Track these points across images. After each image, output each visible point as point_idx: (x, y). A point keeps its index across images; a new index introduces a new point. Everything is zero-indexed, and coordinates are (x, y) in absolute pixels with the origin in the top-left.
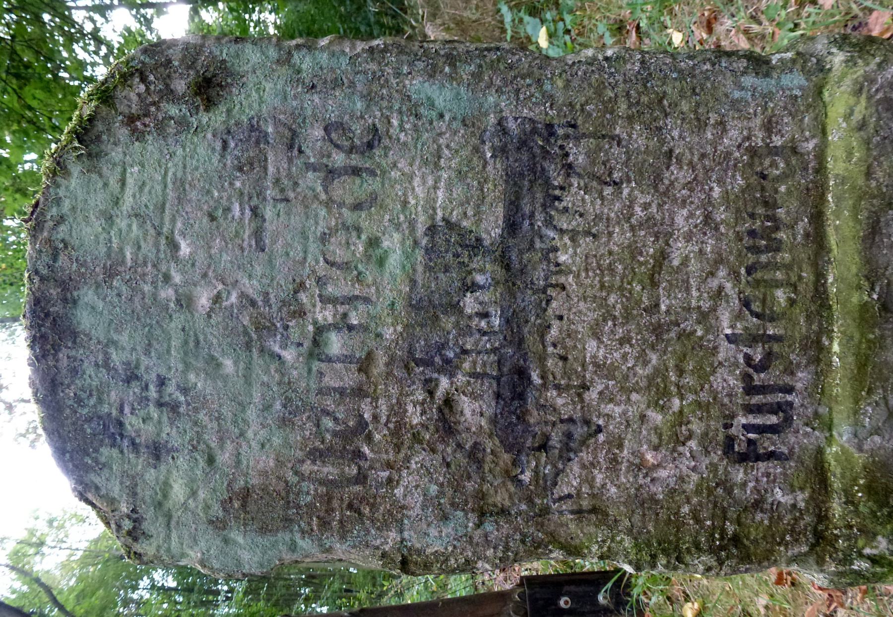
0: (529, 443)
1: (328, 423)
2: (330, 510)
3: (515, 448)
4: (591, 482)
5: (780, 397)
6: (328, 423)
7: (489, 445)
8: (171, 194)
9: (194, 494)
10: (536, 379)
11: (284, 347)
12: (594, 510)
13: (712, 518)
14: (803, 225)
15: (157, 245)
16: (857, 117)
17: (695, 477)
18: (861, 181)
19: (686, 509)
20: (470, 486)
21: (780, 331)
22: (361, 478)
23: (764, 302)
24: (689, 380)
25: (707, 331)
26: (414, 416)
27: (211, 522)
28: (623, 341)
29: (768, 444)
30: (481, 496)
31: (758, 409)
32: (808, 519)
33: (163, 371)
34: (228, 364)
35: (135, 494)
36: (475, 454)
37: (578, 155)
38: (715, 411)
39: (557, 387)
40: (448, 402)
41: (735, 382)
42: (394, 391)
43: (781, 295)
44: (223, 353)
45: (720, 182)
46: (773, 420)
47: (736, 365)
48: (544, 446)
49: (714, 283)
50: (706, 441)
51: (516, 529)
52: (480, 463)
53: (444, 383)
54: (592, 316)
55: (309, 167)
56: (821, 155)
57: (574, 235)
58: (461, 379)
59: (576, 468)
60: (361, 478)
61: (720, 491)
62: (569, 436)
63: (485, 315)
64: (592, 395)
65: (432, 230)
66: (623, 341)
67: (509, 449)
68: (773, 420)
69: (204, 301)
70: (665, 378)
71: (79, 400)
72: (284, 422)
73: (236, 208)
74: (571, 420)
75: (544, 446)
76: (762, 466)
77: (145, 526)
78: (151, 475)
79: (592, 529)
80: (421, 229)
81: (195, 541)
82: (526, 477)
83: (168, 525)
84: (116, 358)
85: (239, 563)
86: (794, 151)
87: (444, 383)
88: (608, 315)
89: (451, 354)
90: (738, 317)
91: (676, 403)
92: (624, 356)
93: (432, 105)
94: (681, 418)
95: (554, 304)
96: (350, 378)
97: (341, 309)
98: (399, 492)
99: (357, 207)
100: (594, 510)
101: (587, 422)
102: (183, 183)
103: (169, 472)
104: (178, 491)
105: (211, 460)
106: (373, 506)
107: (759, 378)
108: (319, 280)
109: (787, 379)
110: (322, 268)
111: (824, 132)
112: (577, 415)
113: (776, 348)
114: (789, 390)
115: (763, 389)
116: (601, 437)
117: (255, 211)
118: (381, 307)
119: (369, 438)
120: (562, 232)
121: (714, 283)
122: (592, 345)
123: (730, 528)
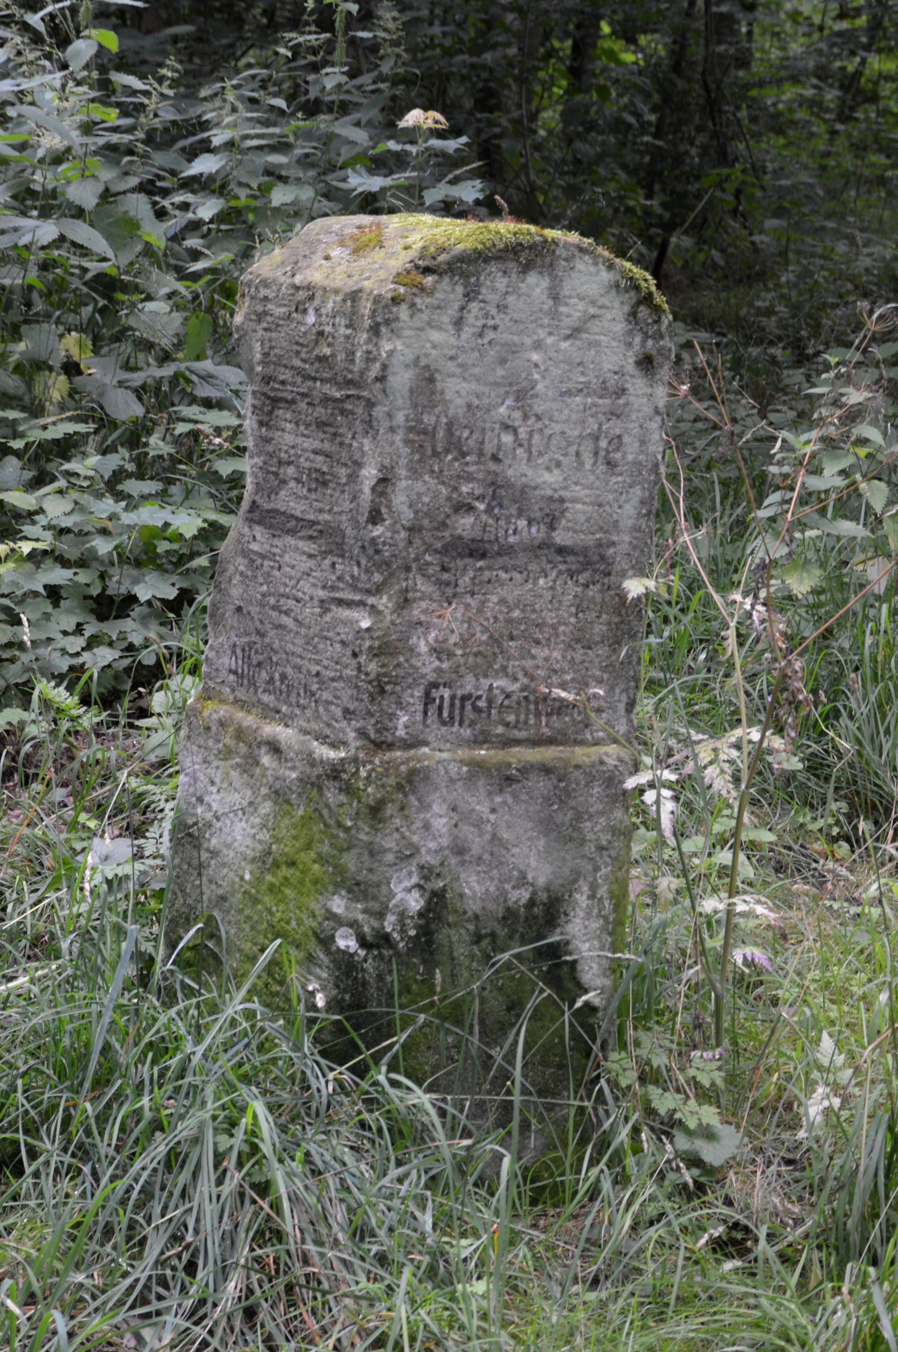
0: (446, 560)
1: (466, 434)
2: (419, 433)
3: (444, 551)
4: (422, 599)
5: (457, 718)
6: (466, 434)
7: (447, 534)
9: (434, 347)
10: (480, 564)
14: (546, 731)
16: (606, 759)
17: (419, 664)
18: (574, 763)
22: (435, 454)
23: (508, 707)
24: (471, 659)
25: (496, 672)
28: (496, 618)
29: (432, 710)
31: (452, 705)
36: (444, 525)
38: (454, 676)
39: (475, 577)
40: (471, 508)
41: (469, 688)
43: (511, 718)
45: (573, 680)
46: (445, 714)
47: (477, 689)
48: (444, 569)
49: (520, 675)
52: (437, 529)
53: (482, 507)
54: (510, 598)
55: (601, 425)
56: (583, 743)
58: (484, 517)
59: (430, 589)
62: (448, 584)
63: (515, 532)
65: (562, 500)
66: (496, 618)
68: (445, 714)
69: (535, 357)
72: (469, 406)
74: (456, 585)
76: (421, 708)
78: (446, 319)
80: (562, 493)
82: (428, 558)
84: (511, 299)
85: (394, 374)
86: (587, 726)
87: (482, 507)
88: (510, 610)
89: (496, 511)
90: (503, 691)
91: (459, 652)
92: (487, 619)
93: (626, 501)
94: (450, 655)
95: (518, 576)
96: (489, 448)
98: (427, 478)
100: (406, 600)
101: (454, 596)
104: (436, 336)
105: (452, 358)
107: (469, 707)
109: (467, 723)
110: (548, 432)
111: (595, 744)
112: (459, 590)
113: (484, 715)
114: (461, 724)
115: (463, 707)
117: (581, 390)
119: (456, 459)
120: (555, 581)
121: (520, 675)
122: (495, 599)
123: (388, 688)
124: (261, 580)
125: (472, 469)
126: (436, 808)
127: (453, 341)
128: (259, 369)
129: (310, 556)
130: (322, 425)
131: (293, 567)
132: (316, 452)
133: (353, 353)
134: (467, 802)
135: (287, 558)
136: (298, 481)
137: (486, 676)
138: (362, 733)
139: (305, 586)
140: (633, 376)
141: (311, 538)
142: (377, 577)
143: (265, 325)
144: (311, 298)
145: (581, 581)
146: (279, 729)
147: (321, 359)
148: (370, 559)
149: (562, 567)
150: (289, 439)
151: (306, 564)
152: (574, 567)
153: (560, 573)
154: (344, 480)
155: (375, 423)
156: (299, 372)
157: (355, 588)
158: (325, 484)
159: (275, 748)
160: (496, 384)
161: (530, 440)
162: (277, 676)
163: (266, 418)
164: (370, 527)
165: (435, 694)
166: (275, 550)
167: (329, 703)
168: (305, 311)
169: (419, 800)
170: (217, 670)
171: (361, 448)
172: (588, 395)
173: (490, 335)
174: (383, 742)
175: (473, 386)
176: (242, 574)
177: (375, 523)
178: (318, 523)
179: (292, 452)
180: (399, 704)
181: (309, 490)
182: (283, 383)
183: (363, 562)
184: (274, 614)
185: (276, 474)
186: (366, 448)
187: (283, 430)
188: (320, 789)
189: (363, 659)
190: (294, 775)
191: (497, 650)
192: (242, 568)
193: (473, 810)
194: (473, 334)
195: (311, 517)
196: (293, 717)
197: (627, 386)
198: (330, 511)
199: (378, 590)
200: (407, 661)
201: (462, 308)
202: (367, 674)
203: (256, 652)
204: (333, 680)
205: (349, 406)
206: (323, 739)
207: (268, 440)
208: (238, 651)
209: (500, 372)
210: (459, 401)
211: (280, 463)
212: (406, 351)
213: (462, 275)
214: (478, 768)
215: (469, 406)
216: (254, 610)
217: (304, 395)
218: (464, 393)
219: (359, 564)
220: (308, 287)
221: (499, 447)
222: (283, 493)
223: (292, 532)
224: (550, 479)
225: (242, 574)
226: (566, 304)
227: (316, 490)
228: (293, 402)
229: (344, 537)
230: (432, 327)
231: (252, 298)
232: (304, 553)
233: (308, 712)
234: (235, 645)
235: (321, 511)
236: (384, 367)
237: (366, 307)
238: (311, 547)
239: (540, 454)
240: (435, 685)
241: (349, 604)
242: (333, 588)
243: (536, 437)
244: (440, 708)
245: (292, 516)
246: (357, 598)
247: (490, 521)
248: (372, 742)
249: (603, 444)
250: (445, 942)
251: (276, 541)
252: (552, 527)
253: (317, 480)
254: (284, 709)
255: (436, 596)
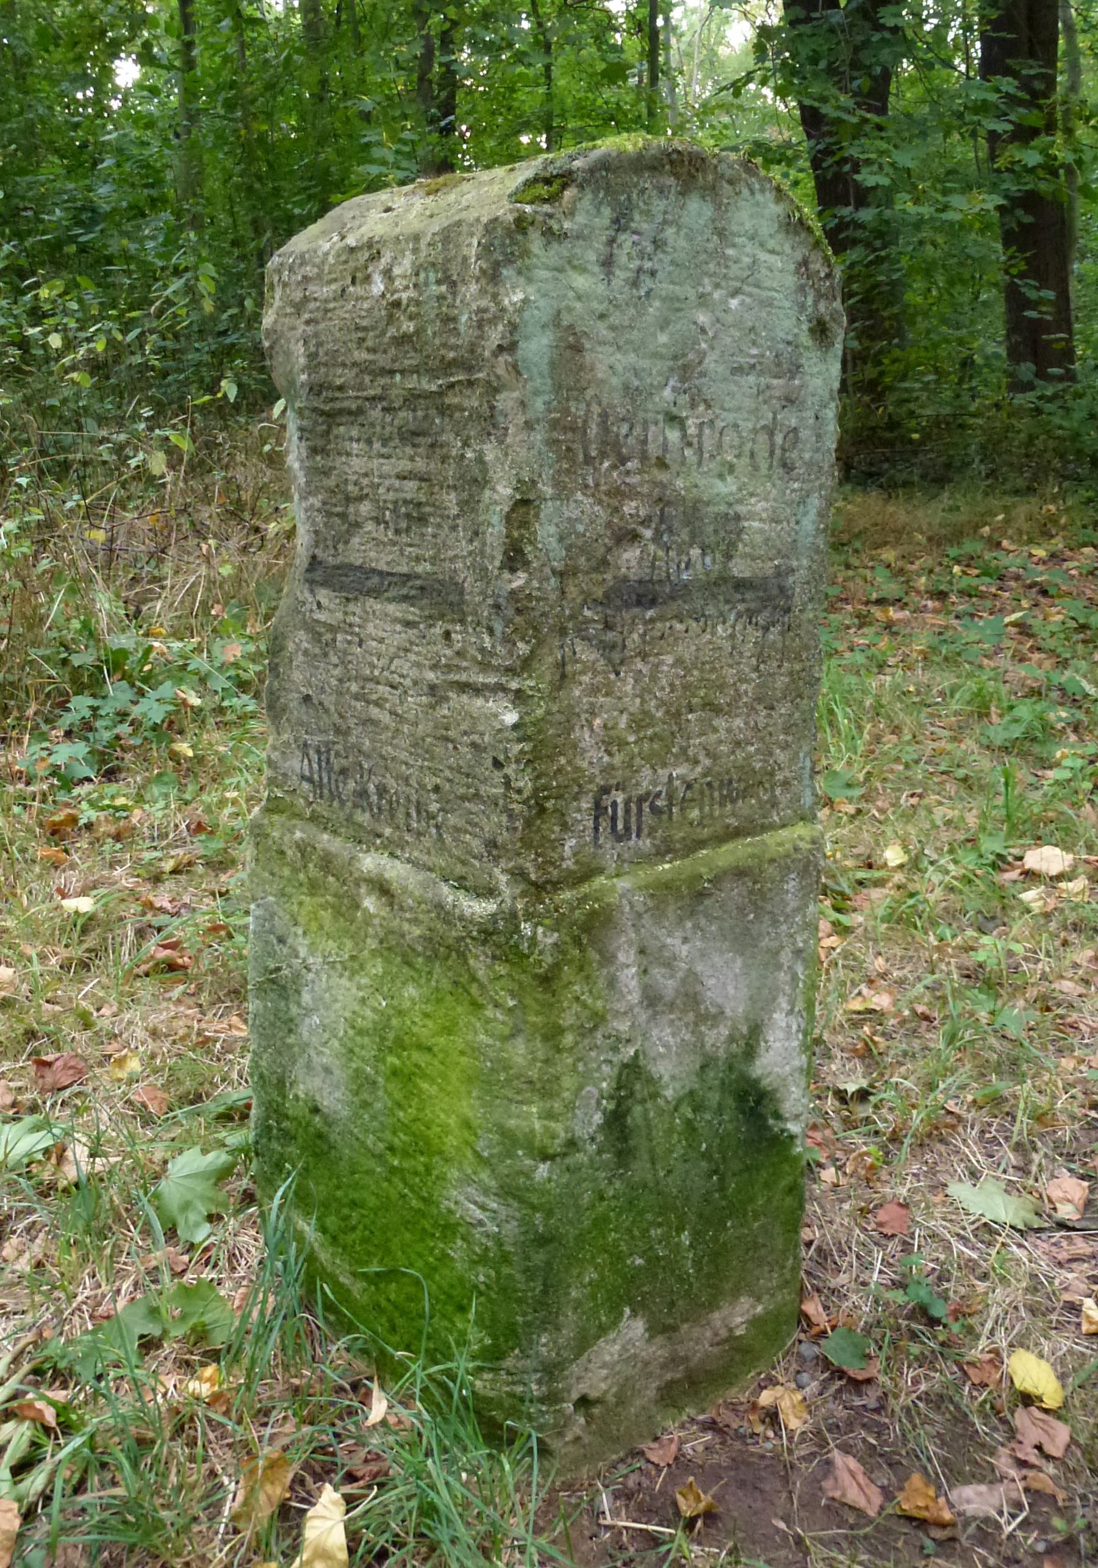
2: (565, 429)
5: (634, 828)
7: (608, 576)
8: (765, 294)
10: (650, 614)
11: (674, 389)
12: (563, 676)
13: (558, 787)
14: (733, 822)
15: (736, 279)
18: (768, 856)
19: (563, 760)
20: (582, 560)
21: (675, 817)
22: (588, 460)
25: (676, 756)
26: (630, 507)
27: (559, 312)
29: (604, 824)
30: (574, 572)
31: (627, 811)
32: (555, 873)
33: (659, 275)
34: (663, 338)
35: (578, 237)
36: (604, 563)
37: (774, 635)
40: (635, 537)
41: (645, 786)
42: (645, 489)
44: (672, 334)
46: (620, 826)
47: (655, 785)
48: (608, 626)
50: (608, 770)
51: (552, 607)
52: (596, 570)
53: (648, 533)
56: (772, 827)
57: (732, 636)
58: (652, 548)
59: (592, 657)
60: (588, 460)
61: (576, 789)
62: (613, 647)
64: (639, 665)
65: (738, 517)
67: (606, 595)
68: (620, 826)
69: (703, 318)
70: (648, 725)
71: (643, 191)
72: (626, 387)
73: (754, 351)
75: (608, 626)
76: (591, 824)
77: (555, 245)
78: (592, 256)
79: (548, 678)
81: (545, 295)
82: (587, 613)
83: (556, 269)
84: (670, 231)
85: (527, 338)
87: (648, 533)
88: (688, 671)
89: (665, 538)
91: (632, 739)
94: (622, 744)
96: (653, 450)
97: (695, 441)
98: (579, 496)
99: (752, 455)
100: (563, 676)
101: (622, 663)
102: (771, 305)
103: (594, 274)
104: (580, 282)
105: (602, 316)
106: (568, 471)
107: (646, 807)
108: (712, 421)
109: (646, 831)
111: (783, 826)
112: (627, 653)
113: (665, 817)
114: (638, 836)
116: (612, 676)
117: (753, 366)
118: (696, 477)
119: (614, 467)
122: (669, 659)
123: (549, 804)
124: (335, 660)
125: (634, 480)
126: (622, 957)
127: (601, 288)
128: (304, 377)
129: (408, 624)
130: (410, 436)
131: (381, 641)
132: (402, 477)
133: (454, 319)
134: (657, 938)
135: (370, 629)
136: (378, 521)
137: (664, 765)
138: (519, 874)
139: (402, 665)
140: (807, 348)
141: (405, 598)
142: (523, 648)
143: (307, 316)
144: (376, 256)
145: (761, 622)
146: (384, 860)
147: (403, 340)
148: (508, 622)
149: (741, 607)
150: (357, 464)
151: (399, 636)
152: (753, 606)
153: (739, 616)
154: (455, 511)
155: (501, 419)
156: (363, 368)
157: (485, 666)
158: (422, 520)
159: (382, 888)
160: (656, 355)
161: (700, 436)
162: (371, 788)
163: (320, 443)
164: (506, 575)
165: (607, 801)
166: (351, 619)
167: (457, 830)
168: (368, 279)
169: (600, 952)
170: (285, 775)
171: (480, 460)
172: (761, 373)
173: (647, 283)
174: (547, 882)
175: (632, 358)
176: (306, 653)
177: (513, 570)
178: (418, 577)
179: (365, 481)
180: (565, 827)
181: (397, 532)
182: (341, 388)
183: (498, 627)
184: (359, 705)
185: (343, 516)
186: (489, 457)
187: (348, 454)
188: (462, 956)
189: (510, 770)
190: (417, 932)
191: (675, 728)
192: (305, 645)
193: (664, 946)
194: (626, 280)
195: (404, 569)
196: (402, 845)
197: (803, 361)
198: (433, 560)
199: (526, 664)
200: (569, 762)
201: (611, 241)
202: (519, 791)
203: (337, 755)
204: (463, 798)
205: (452, 399)
206: (461, 884)
207: (326, 473)
208: (311, 752)
209: (663, 338)
210: (615, 381)
211: (348, 500)
212: (542, 303)
213: (608, 189)
214: (662, 891)
215: (626, 387)
216: (329, 700)
217: (373, 399)
218: (619, 368)
219: (491, 631)
220: (370, 244)
221: (665, 446)
222: (355, 540)
223: (376, 593)
224: (727, 487)
225: (306, 653)
226: (734, 246)
227: (408, 530)
228: (360, 411)
229: (462, 593)
230: (574, 268)
231: (285, 285)
232: (396, 620)
233: (427, 842)
234: (305, 745)
235: (418, 559)
236: (513, 327)
237: (471, 248)
238: (413, 612)
239: (712, 456)
240: (605, 790)
241: (478, 690)
242: (449, 668)
243: (707, 431)
244: (614, 819)
245: (374, 571)
246: (492, 680)
247: (660, 553)
248: (534, 884)
249: (779, 439)
250: (640, 1121)
251: (351, 607)
252: (729, 557)
253: (408, 516)
254: (388, 832)
255: (601, 664)
